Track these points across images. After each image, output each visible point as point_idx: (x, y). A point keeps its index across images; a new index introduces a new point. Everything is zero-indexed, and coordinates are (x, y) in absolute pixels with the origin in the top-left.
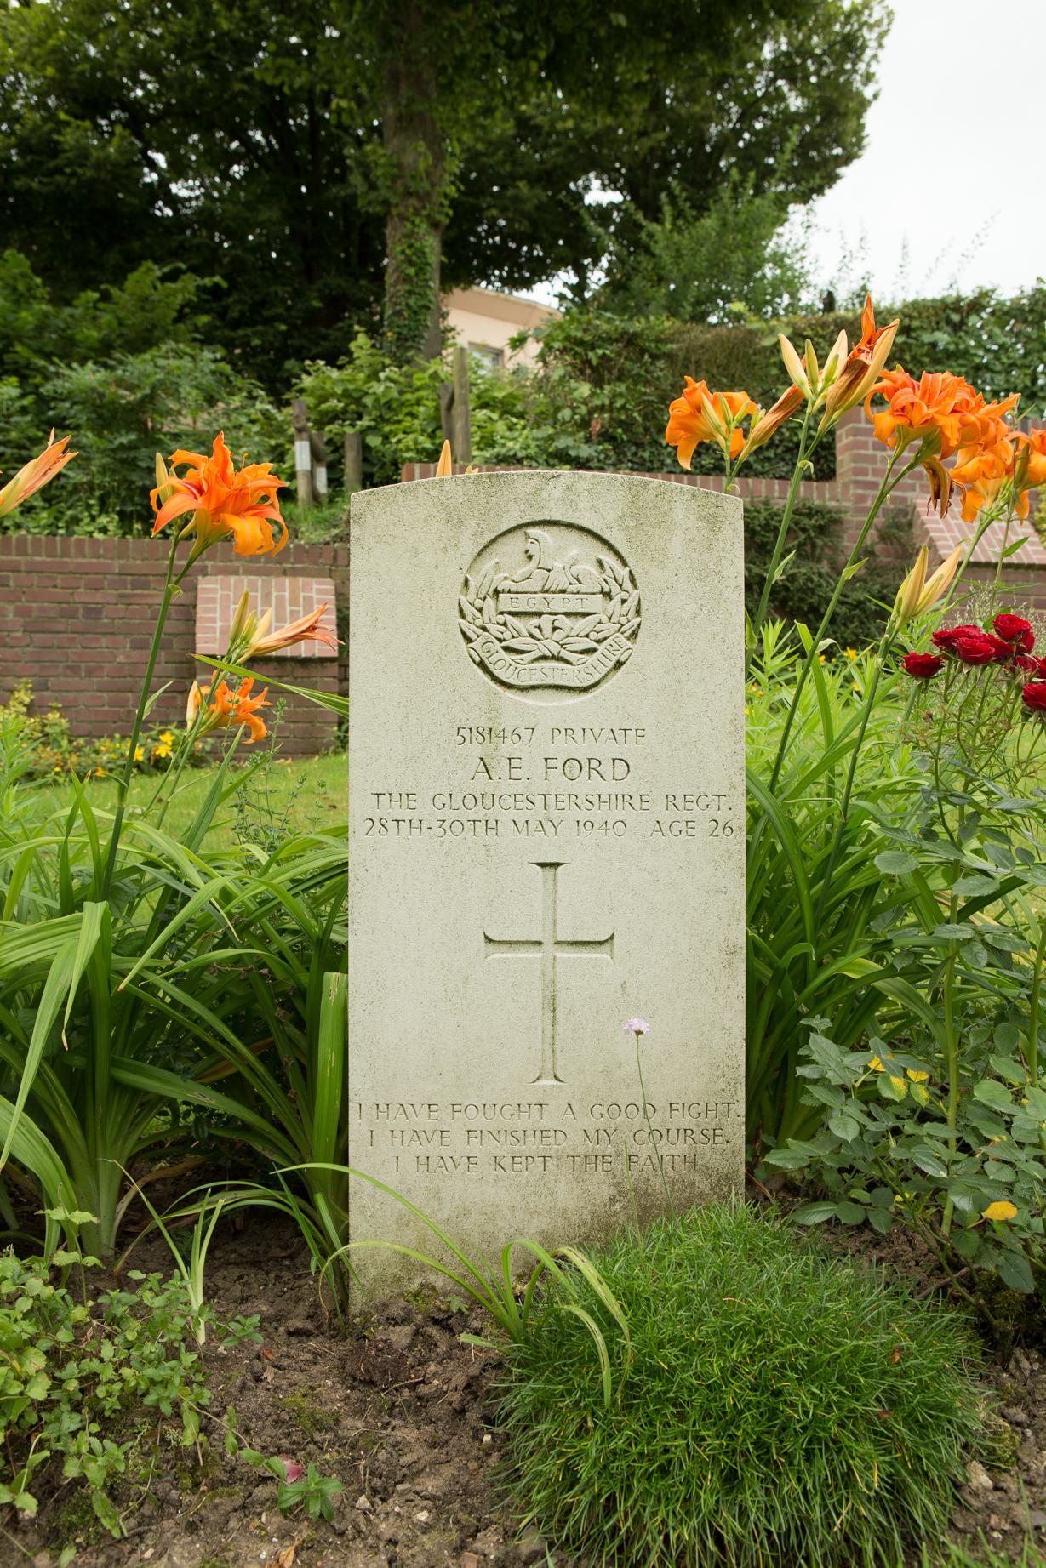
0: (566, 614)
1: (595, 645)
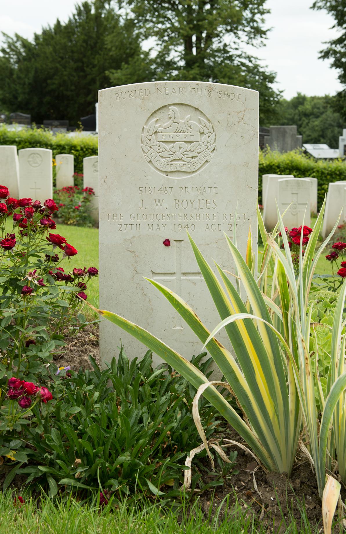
0: (185, 142)
1: (197, 154)
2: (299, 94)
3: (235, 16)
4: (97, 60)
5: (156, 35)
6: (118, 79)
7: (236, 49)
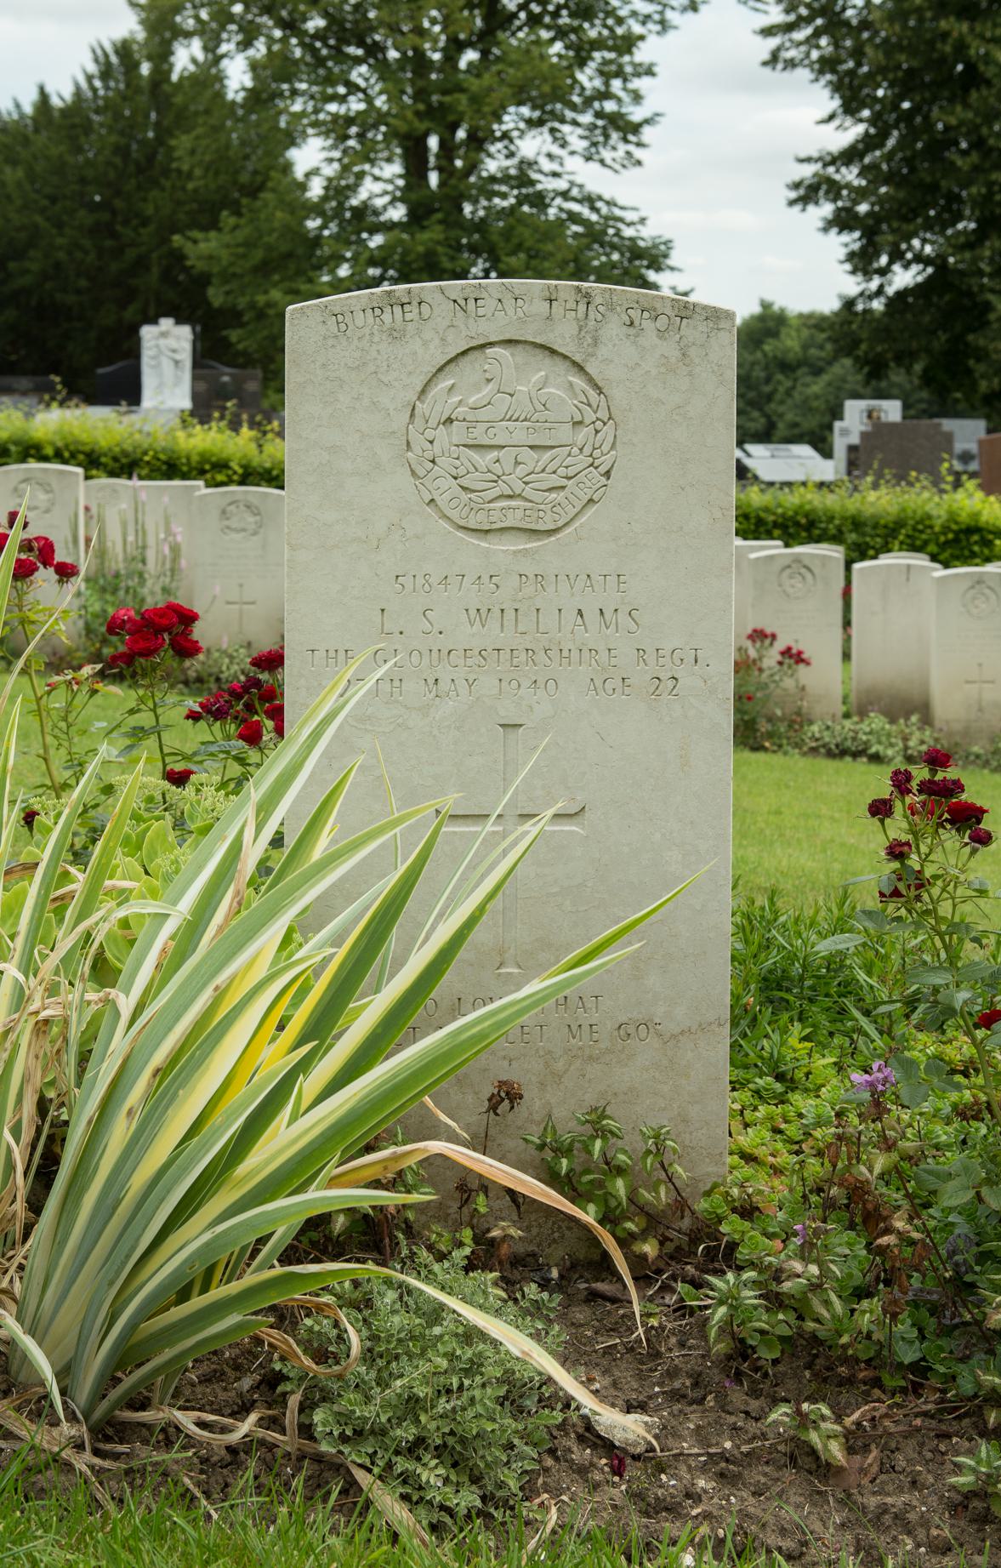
0: (531, 447)
1: (564, 482)
2: (766, 305)
3: (545, 80)
4: (155, 203)
5: (327, 134)
6: (211, 257)
7: (555, 175)
